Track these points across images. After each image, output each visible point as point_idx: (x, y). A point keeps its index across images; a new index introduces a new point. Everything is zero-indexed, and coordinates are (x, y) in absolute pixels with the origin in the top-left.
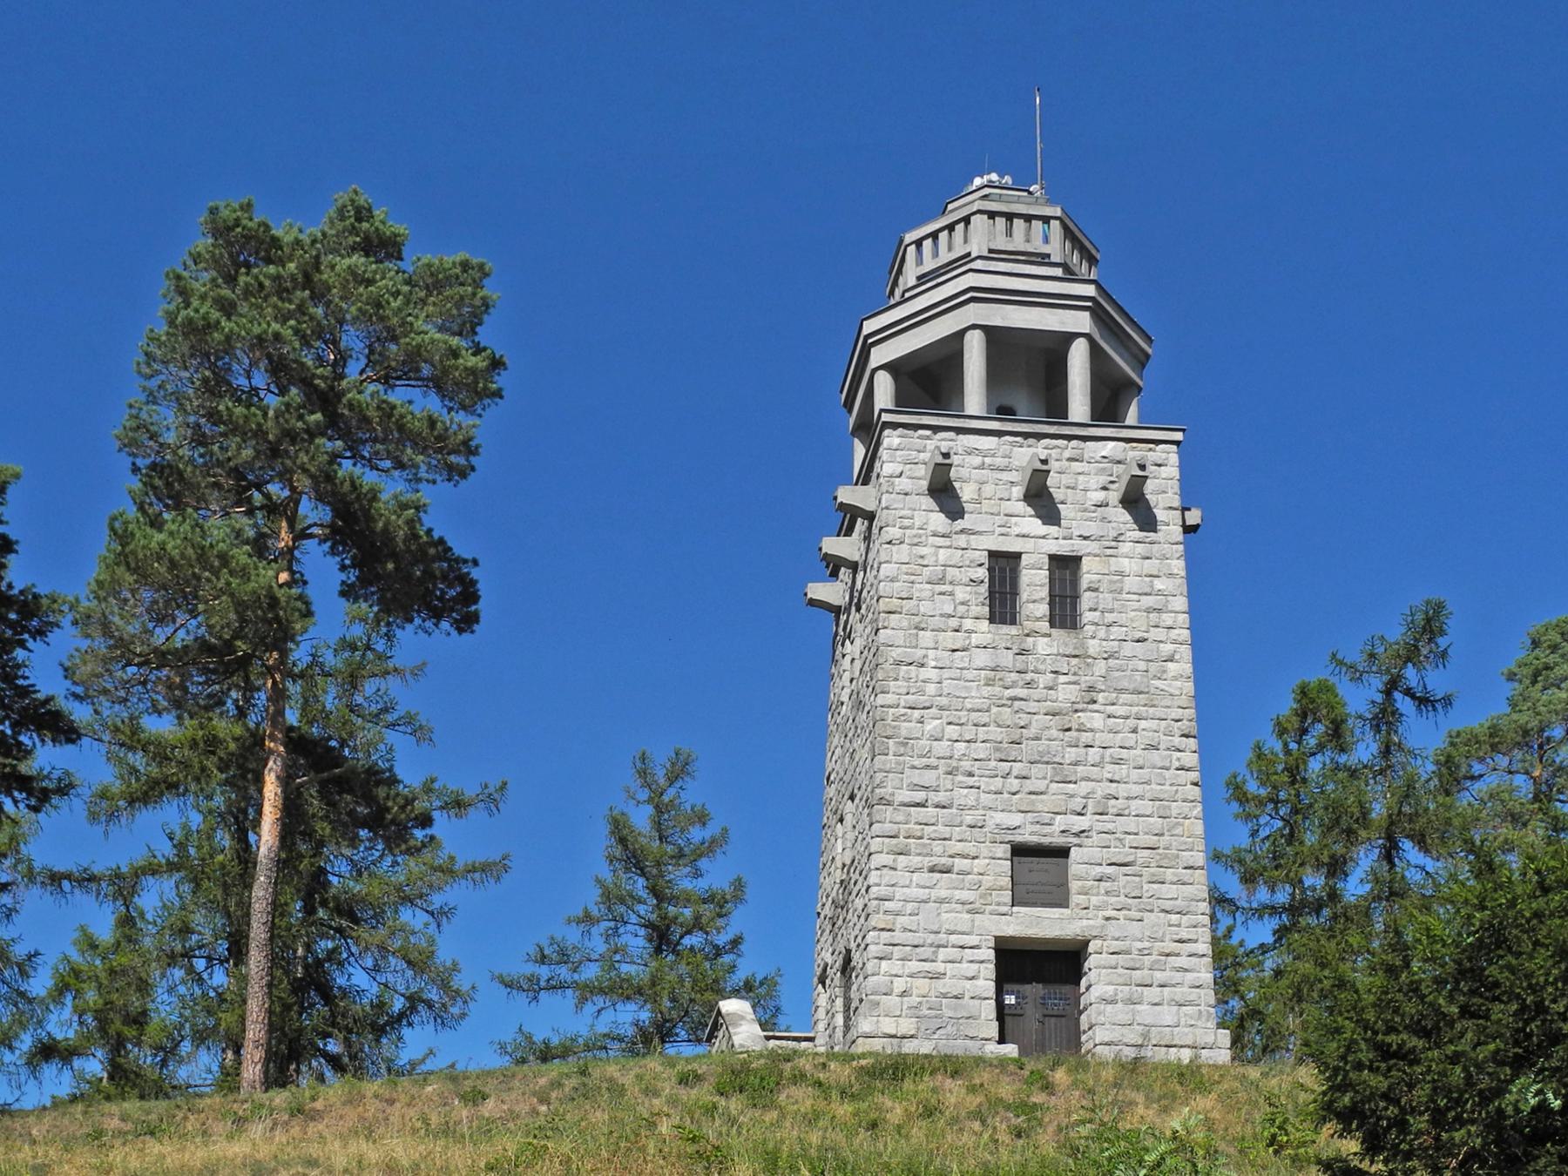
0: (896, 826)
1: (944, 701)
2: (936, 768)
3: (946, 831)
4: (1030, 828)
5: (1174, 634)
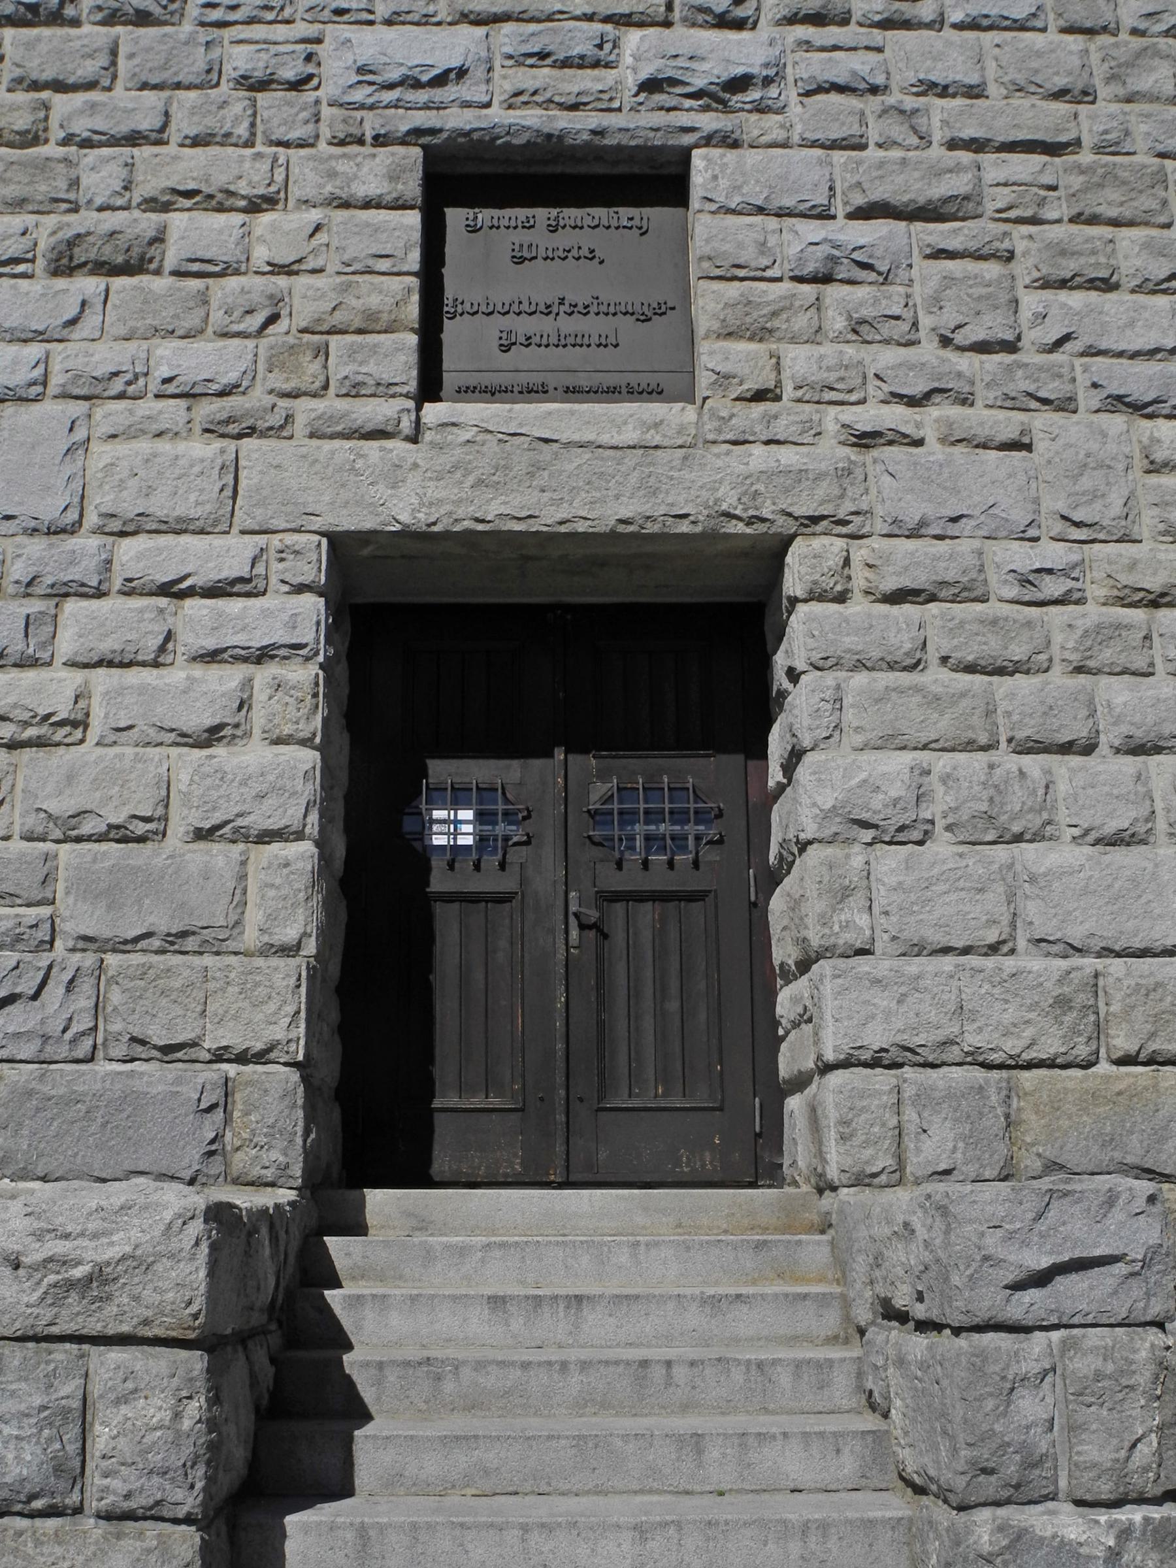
4: (508, 80)
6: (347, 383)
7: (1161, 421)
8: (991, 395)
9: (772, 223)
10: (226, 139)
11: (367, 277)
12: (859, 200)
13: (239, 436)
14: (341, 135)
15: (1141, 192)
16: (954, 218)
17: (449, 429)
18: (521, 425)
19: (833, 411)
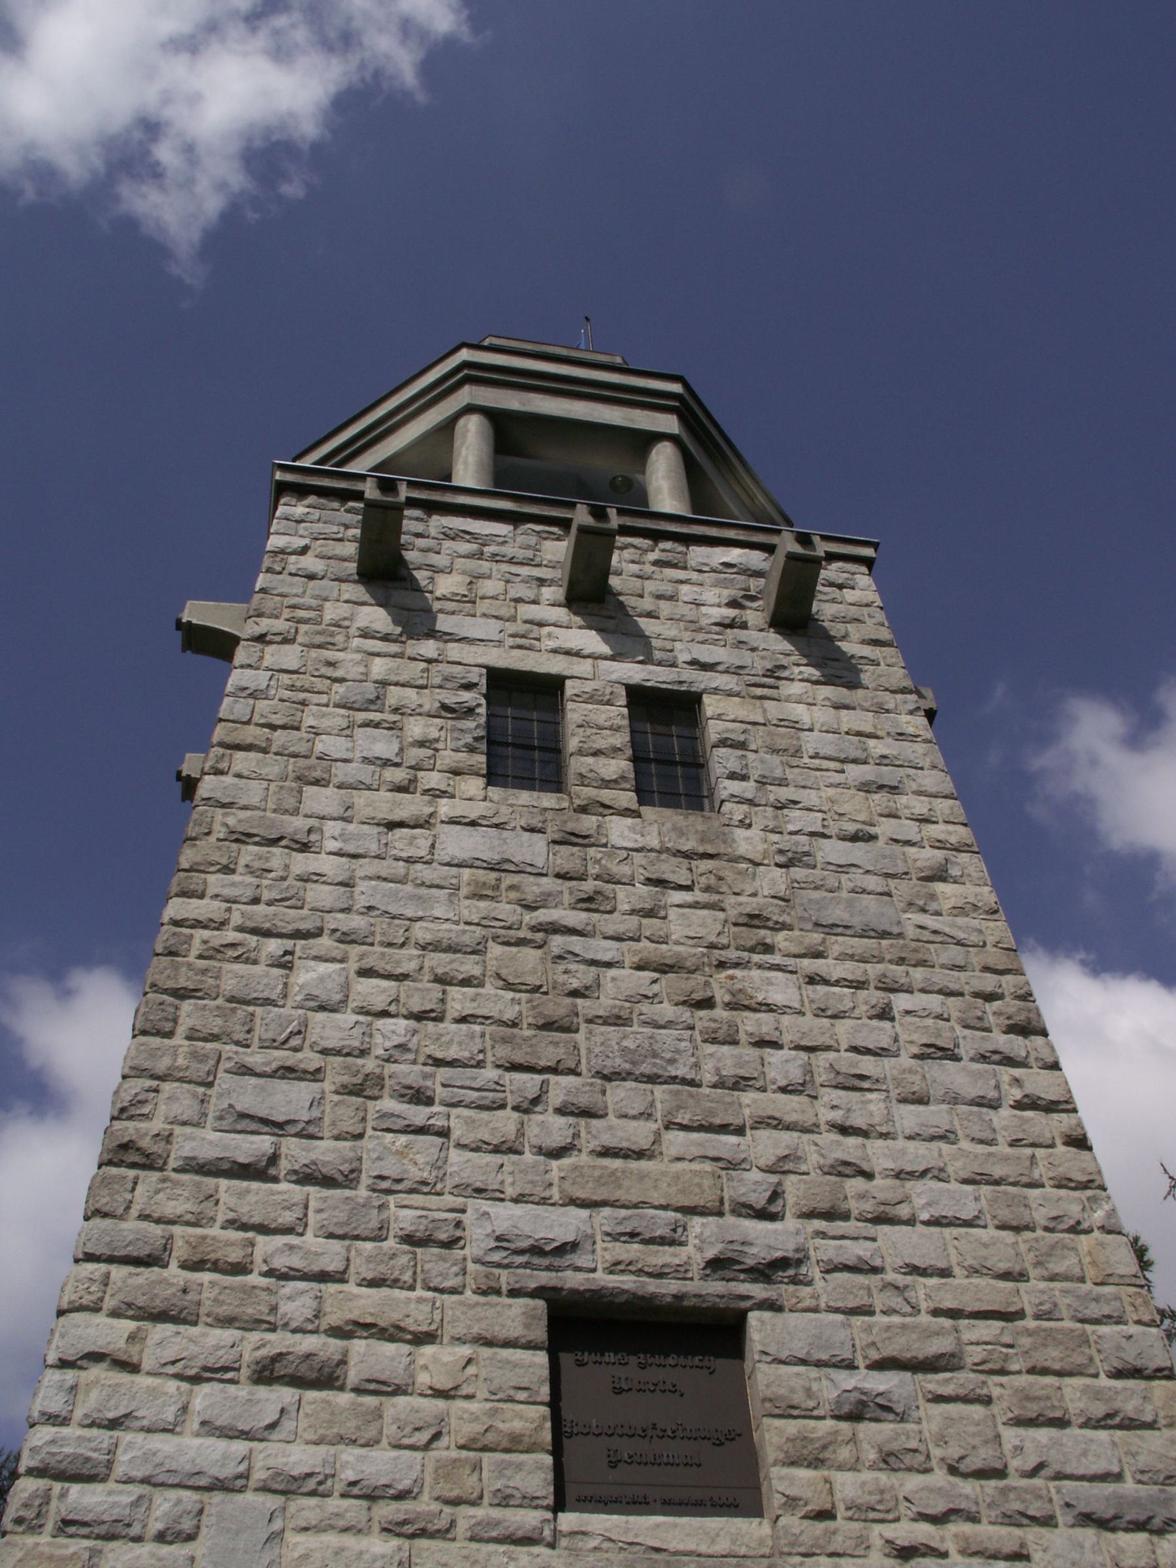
0: (157, 1230)
1: (356, 922)
2: (316, 1075)
3: (331, 1255)
5: (936, 831)
6: (499, 1495)
7: (1121, 1534)
8: (993, 1513)
9: (813, 1372)
10: (395, 1283)
11: (509, 1405)
12: (875, 1355)
13: (413, 1536)
14: (484, 1287)
15: (1073, 1350)
16: (946, 1370)
17: (579, 1537)
18: (636, 1535)
19: (877, 1528)
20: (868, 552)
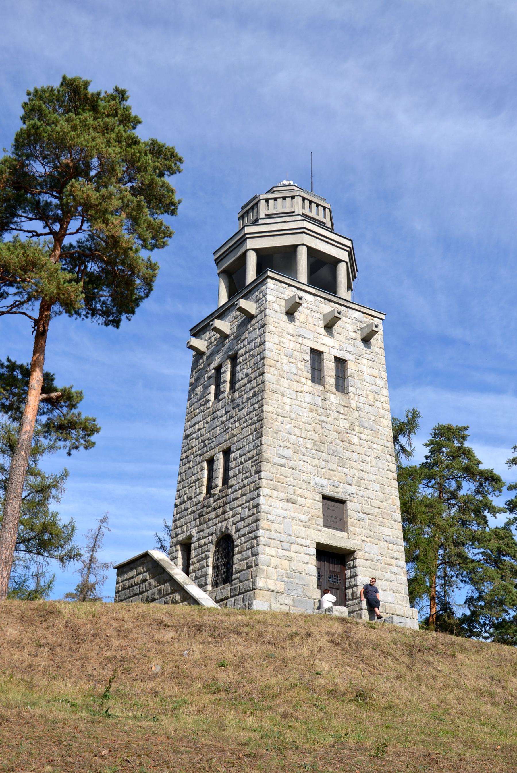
9: (355, 512)
20: (383, 317)
